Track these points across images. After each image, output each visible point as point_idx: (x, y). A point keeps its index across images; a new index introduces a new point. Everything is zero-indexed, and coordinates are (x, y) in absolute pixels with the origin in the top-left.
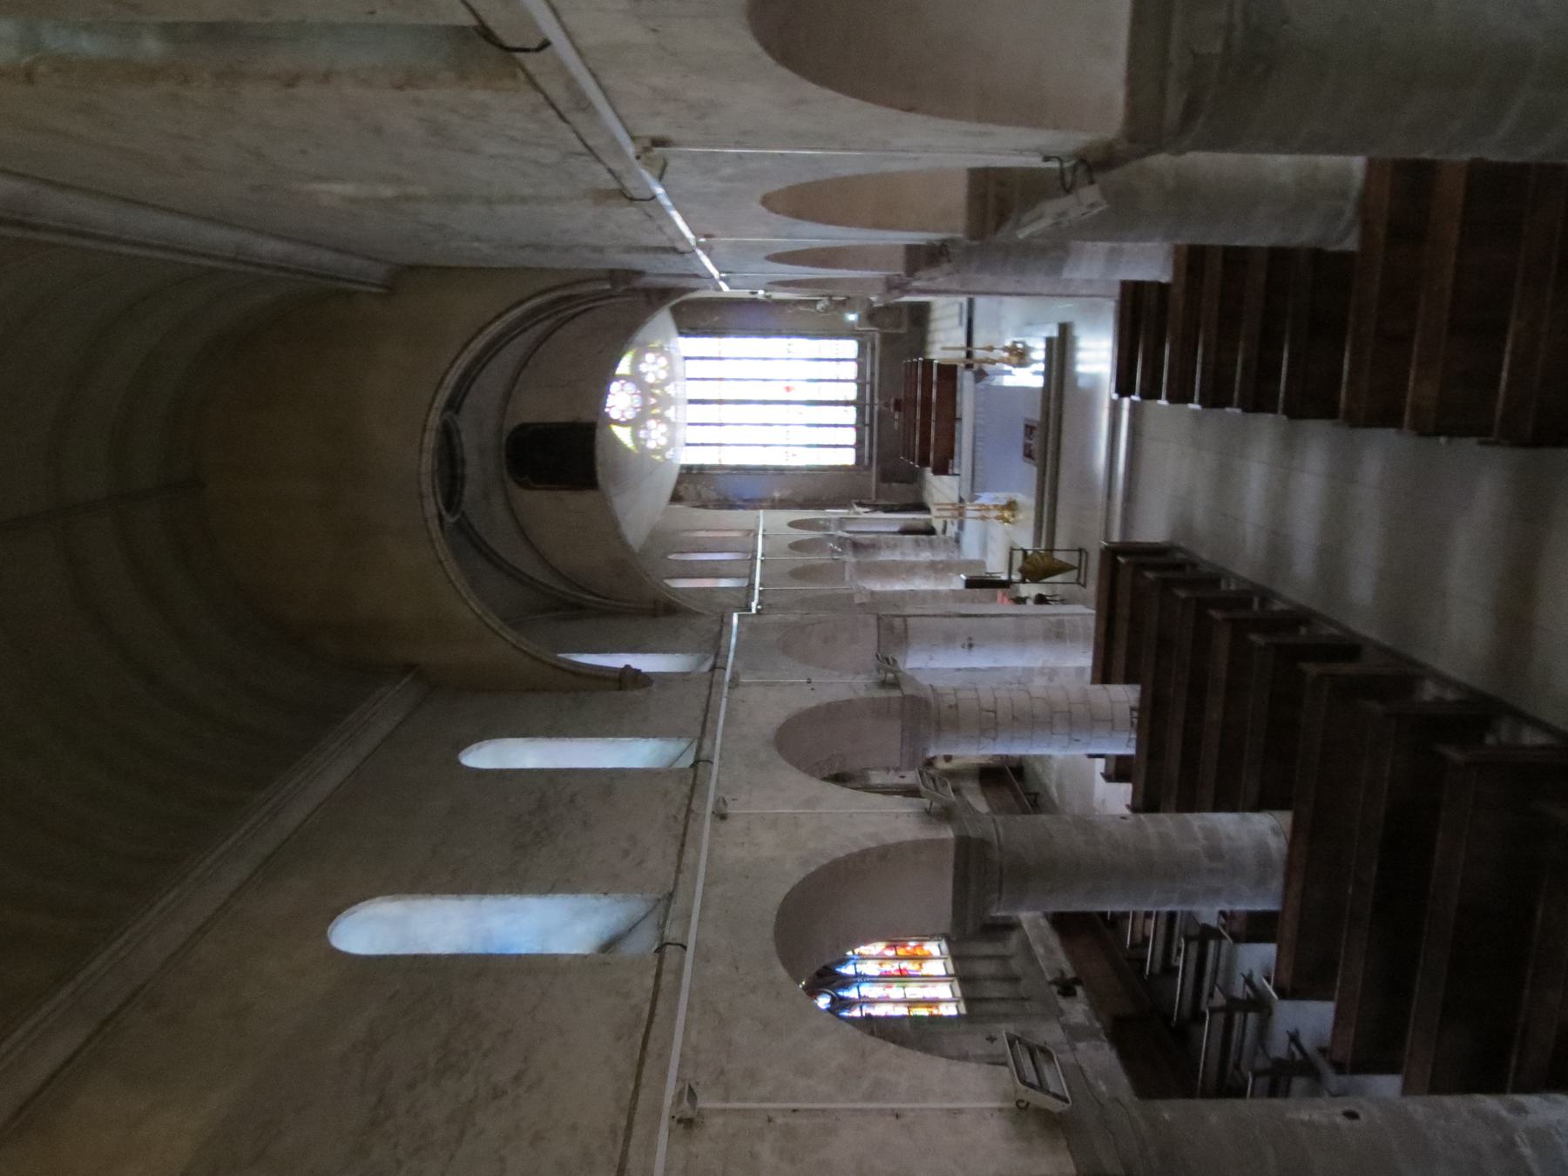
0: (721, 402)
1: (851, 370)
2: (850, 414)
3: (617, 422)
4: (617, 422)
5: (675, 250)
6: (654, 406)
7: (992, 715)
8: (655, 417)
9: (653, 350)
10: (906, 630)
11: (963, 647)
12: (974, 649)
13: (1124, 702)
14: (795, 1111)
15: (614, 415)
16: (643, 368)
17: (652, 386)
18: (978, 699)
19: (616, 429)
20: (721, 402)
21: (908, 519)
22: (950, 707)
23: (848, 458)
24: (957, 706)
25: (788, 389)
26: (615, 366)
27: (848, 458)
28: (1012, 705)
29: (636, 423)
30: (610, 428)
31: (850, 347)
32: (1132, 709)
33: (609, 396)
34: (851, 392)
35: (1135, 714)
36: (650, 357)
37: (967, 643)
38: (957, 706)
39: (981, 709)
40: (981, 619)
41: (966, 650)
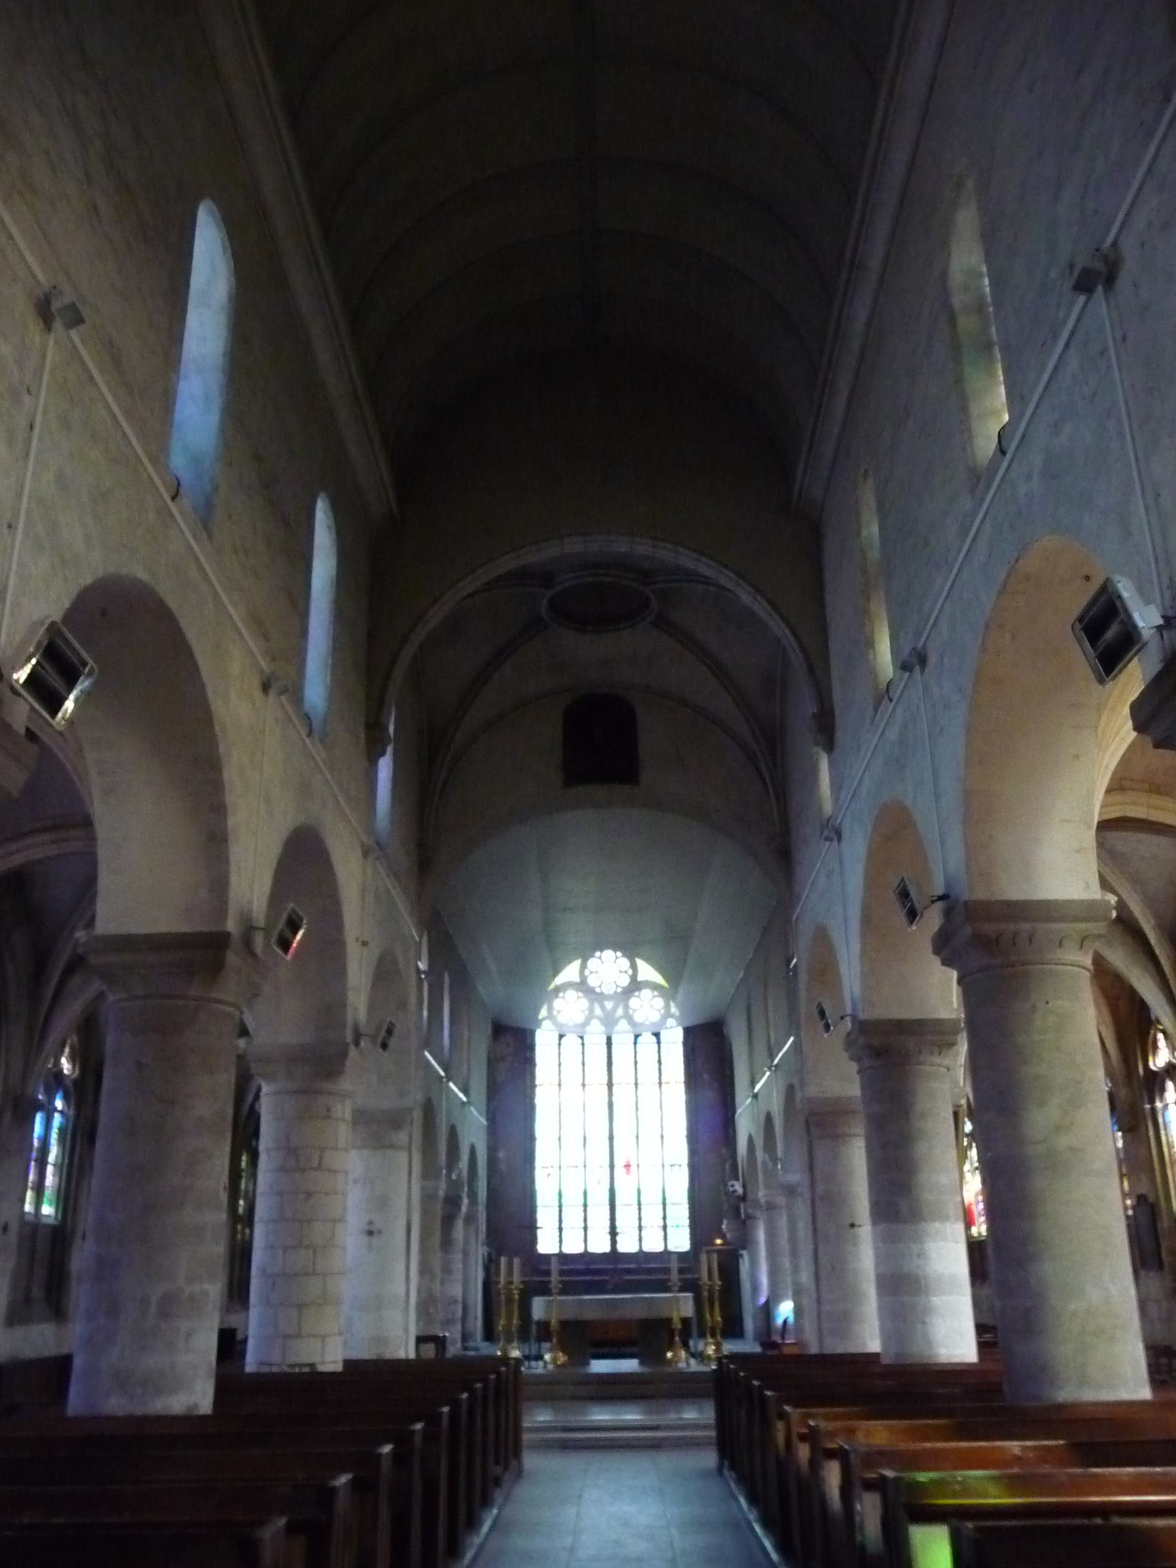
0: (610, 1085)
1: (653, 1244)
2: (600, 1245)
3: (583, 967)
4: (583, 967)
5: (829, 819)
6: (603, 1007)
7: (315, 1165)
8: (591, 1010)
9: (667, 1007)
10: (392, 1146)
11: (370, 1223)
12: (366, 1238)
13: (323, 1355)
14: (31, 427)
15: (592, 963)
16: (646, 993)
17: (627, 1007)
18: (335, 1148)
19: (577, 964)
20: (610, 1085)
21: (476, 1309)
22: (328, 1110)
23: (546, 1244)
24: (328, 1117)
25: (628, 1166)
26: (542, 1375)
27: (546, 1244)
28: (327, 1194)
29: (582, 986)
30: (578, 959)
31: (681, 1241)
32: (312, 1365)
33: (539, 1231)
34: (627, 1245)
35: (306, 1370)
36: (659, 1002)
37: (374, 1228)
38: (328, 1117)
39: (322, 1150)
40: (404, 1252)
41: (366, 1228)
